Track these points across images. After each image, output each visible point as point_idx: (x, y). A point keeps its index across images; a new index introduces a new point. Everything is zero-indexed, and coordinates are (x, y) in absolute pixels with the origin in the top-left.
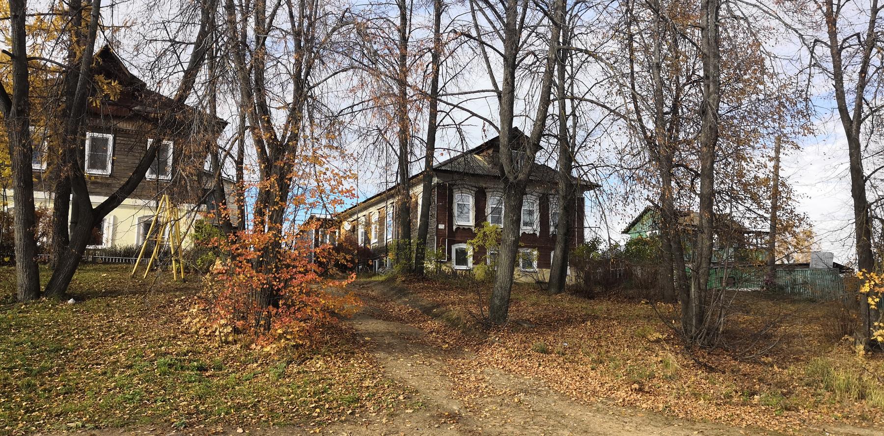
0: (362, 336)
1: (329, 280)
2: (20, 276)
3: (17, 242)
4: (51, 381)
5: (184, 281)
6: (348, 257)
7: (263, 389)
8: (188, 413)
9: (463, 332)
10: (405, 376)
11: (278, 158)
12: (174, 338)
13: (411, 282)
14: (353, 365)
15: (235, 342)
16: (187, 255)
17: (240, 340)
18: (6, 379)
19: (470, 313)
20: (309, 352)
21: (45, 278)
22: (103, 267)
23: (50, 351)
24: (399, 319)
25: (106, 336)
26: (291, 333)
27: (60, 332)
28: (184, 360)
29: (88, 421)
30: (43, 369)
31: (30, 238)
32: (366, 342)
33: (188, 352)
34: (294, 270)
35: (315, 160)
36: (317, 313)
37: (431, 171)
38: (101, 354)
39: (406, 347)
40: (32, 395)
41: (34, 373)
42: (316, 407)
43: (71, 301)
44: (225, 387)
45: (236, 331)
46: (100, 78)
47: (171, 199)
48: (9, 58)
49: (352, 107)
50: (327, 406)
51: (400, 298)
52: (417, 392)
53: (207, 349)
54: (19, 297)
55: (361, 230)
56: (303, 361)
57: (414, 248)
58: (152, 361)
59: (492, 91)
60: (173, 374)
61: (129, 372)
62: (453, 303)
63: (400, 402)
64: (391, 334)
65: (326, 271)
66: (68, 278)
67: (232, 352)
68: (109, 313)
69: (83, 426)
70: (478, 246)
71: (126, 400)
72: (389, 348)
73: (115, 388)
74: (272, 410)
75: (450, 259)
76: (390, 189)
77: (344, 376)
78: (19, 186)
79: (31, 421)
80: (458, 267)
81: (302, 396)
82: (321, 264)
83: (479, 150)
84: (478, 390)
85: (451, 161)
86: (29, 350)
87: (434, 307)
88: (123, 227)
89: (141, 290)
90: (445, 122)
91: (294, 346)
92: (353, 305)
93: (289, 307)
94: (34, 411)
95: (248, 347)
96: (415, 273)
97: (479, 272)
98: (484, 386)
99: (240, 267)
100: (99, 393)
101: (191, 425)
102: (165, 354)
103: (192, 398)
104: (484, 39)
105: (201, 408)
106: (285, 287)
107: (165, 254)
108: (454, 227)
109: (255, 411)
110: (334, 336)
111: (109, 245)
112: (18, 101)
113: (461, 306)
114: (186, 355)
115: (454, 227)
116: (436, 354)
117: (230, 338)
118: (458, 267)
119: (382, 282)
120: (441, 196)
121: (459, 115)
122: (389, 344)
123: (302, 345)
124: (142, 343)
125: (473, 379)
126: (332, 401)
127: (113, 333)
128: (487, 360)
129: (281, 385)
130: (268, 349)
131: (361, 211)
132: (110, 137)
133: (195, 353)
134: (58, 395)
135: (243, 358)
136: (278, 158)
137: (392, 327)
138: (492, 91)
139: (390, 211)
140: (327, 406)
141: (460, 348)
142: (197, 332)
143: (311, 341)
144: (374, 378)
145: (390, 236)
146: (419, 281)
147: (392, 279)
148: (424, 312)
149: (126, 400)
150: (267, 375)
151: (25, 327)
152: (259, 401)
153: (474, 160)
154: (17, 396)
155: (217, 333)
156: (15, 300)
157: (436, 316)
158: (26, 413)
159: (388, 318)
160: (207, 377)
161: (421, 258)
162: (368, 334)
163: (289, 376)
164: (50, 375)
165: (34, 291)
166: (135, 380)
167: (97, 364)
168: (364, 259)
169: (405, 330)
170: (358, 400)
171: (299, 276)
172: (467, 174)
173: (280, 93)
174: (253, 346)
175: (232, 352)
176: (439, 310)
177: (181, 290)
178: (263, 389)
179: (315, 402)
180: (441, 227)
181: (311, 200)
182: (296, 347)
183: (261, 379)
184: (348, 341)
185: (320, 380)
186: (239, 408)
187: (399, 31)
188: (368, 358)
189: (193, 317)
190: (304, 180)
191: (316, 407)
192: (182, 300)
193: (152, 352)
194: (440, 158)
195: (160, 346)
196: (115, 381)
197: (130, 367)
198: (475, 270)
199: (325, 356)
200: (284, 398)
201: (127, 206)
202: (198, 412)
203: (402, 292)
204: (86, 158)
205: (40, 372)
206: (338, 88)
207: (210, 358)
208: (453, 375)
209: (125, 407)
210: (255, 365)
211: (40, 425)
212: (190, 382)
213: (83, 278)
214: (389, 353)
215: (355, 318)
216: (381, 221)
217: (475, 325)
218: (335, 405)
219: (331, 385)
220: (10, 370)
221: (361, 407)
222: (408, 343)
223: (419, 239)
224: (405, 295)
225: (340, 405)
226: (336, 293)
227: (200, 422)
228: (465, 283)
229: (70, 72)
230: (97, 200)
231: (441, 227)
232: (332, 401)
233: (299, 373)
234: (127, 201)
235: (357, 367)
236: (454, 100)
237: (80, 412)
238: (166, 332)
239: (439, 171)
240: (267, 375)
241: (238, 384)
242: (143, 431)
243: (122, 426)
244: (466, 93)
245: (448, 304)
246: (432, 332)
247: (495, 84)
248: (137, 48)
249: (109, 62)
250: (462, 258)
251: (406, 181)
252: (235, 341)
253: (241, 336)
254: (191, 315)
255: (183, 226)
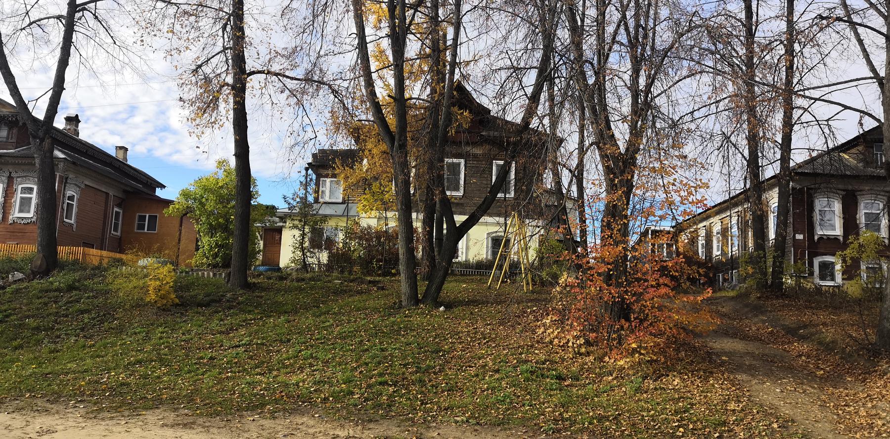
0: (718, 355)
1: (682, 295)
2: (404, 287)
3: (401, 256)
4: (436, 378)
5: (533, 292)
6: (701, 271)
7: (622, 403)
8: (554, 419)
9: (841, 358)
10: (776, 402)
11: (621, 169)
12: (532, 346)
13: (767, 298)
14: (713, 385)
15: (588, 354)
16: (531, 267)
17: (592, 352)
18: (403, 373)
19: (850, 336)
20: (663, 368)
21: (422, 287)
22: (462, 278)
23: (432, 352)
24: (756, 339)
25: (474, 341)
26: (646, 348)
27: (437, 336)
28: (544, 368)
29: (470, 418)
30: (429, 367)
31: (411, 251)
32: (723, 363)
33: (546, 361)
34: (646, 284)
35: (663, 172)
36: (671, 328)
37: (787, 173)
38: (472, 357)
39: (771, 370)
40: (424, 389)
41: (423, 370)
42: (679, 426)
43: (442, 309)
44: (584, 398)
45: (588, 343)
46: (455, 109)
47: (520, 215)
48: (392, 100)
49: (692, 113)
50: (691, 426)
51: (756, 316)
52: (793, 421)
53: (563, 360)
54: (403, 304)
55: (701, 241)
56: (659, 377)
57: (770, 261)
58: (515, 367)
59: (871, 78)
60: (536, 381)
61: (497, 376)
62: (825, 324)
63: (773, 431)
64: (752, 355)
65: (679, 285)
66: (439, 289)
67: (586, 364)
68: (474, 321)
69: (467, 421)
70: (852, 258)
71: (498, 401)
72: (751, 370)
73: (488, 389)
74: (633, 425)
75: (811, 274)
76: (733, 198)
77: (705, 397)
78: (402, 209)
79: (427, 411)
80: (823, 283)
81: (663, 414)
82: (673, 278)
83: (847, 146)
84: (872, 428)
85: (812, 160)
86: (416, 351)
87: (800, 328)
88: (474, 246)
89: (499, 300)
90: (803, 119)
91: (648, 361)
92: (706, 321)
93: (642, 321)
94: (427, 403)
95: (601, 359)
96: (772, 289)
97: (853, 289)
98: (880, 423)
99: (592, 281)
100: (474, 393)
101: (559, 431)
102: (526, 361)
103: (556, 406)
104: (856, 19)
105: (566, 415)
106: (637, 301)
107: (515, 266)
108: (816, 238)
109: (617, 424)
110: (685, 353)
111: (464, 259)
112: (400, 137)
113: (831, 328)
114: (544, 364)
115: (816, 238)
116: (811, 381)
117: (583, 350)
118: (823, 283)
119: (733, 298)
120: (797, 203)
121: (822, 111)
122: (750, 365)
123: (656, 361)
124: (504, 349)
125: (863, 412)
126: (695, 422)
127: (479, 339)
128: (880, 393)
129: (639, 400)
130: (622, 363)
131: (701, 221)
132: (462, 161)
133: (552, 362)
134: (443, 392)
135: (598, 370)
136: (621, 169)
137: (751, 347)
138: (871, 78)
139: (734, 220)
140: (691, 426)
141: (841, 377)
142: (551, 342)
143: (665, 357)
144: (739, 401)
145: (735, 248)
146: (777, 298)
147: (742, 297)
148: (787, 333)
149: (498, 401)
150: (624, 389)
151: (411, 330)
152: (619, 415)
153: (841, 159)
154: (414, 389)
155: (570, 344)
156: (400, 307)
157: (803, 338)
158: (422, 404)
159: (745, 338)
160: (566, 386)
161: (778, 273)
162: (725, 353)
163: (646, 392)
164: (435, 373)
165: (415, 301)
166: (504, 384)
167: (470, 367)
168: (711, 272)
169: (767, 351)
170: (724, 423)
171: (651, 290)
172: (833, 176)
173: (619, 103)
174: (607, 359)
175: (586, 364)
176: (807, 331)
177: (531, 301)
178: (622, 403)
179: (678, 421)
180: (800, 237)
181: (660, 213)
182: (651, 362)
183: (618, 394)
184: (704, 359)
185: (680, 398)
186: (601, 419)
187: (744, 25)
188: (728, 379)
189: (547, 328)
190: (647, 190)
191: (679, 426)
192: (534, 311)
193: (514, 359)
194: (798, 157)
195: (521, 354)
196: (487, 383)
197: (497, 371)
198: (845, 287)
199: (681, 374)
200: (645, 414)
201: (486, 224)
202: (563, 420)
203: (758, 310)
204: (494, 173)
205: (427, 371)
206: (690, 94)
207: (566, 368)
208: (836, 407)
209: (499, 408)
210: (610, 378)
211: (433, 416)
212: (551, 390)
213: (452, 288)
214: (752, 376)
215: (708, 336)
216: (724, 232)
217: (857, 351)
218: (700, 426)
219: (692, 405)
220: (405, 365)
221: (729, 431)
222: (774, 367)
223: (776, 251)
224: (762, 313)
225: (705, 427)
226: (681, 310)
227: (566, 430)
228: (836, 301)
229: (434, 106)
230: (460, 219)
231: (800, 237)
232: (695, 422)
233: (656, 389)
234: (485, 219)
235: (718, 389)
236: (816, 94)
237: (464, 408)
238: (524, 340)
239: (799, 173)
240: (624, 389)
241: (596, 396)
242: (517, 432)
243: (499, 425)
244: (834, 84)
245: (818, 325)
246: (800, 356)
247: (873, 69)
248: (485, 78)
249: (462, 97)
250: (827, 271)
251: (757, 187)
252: (588, 353)
253: (592, 349)
254: (544, 325)
255: (528, 242)
